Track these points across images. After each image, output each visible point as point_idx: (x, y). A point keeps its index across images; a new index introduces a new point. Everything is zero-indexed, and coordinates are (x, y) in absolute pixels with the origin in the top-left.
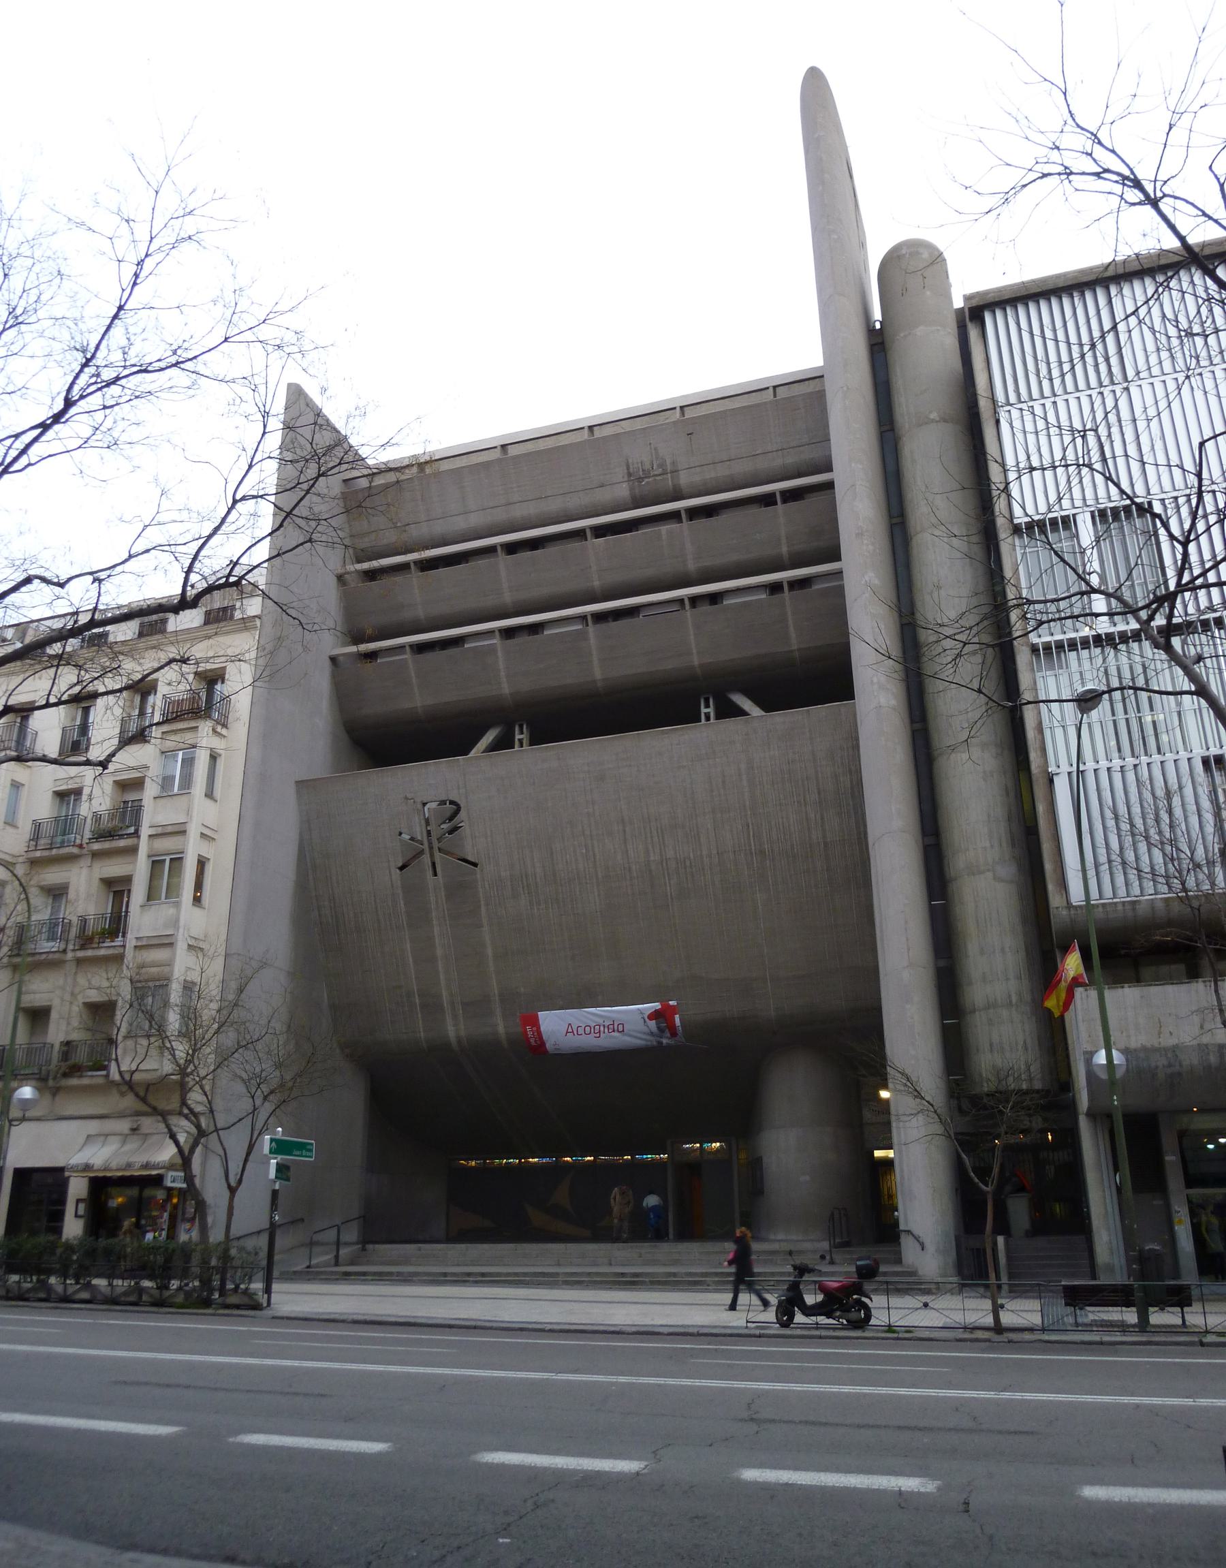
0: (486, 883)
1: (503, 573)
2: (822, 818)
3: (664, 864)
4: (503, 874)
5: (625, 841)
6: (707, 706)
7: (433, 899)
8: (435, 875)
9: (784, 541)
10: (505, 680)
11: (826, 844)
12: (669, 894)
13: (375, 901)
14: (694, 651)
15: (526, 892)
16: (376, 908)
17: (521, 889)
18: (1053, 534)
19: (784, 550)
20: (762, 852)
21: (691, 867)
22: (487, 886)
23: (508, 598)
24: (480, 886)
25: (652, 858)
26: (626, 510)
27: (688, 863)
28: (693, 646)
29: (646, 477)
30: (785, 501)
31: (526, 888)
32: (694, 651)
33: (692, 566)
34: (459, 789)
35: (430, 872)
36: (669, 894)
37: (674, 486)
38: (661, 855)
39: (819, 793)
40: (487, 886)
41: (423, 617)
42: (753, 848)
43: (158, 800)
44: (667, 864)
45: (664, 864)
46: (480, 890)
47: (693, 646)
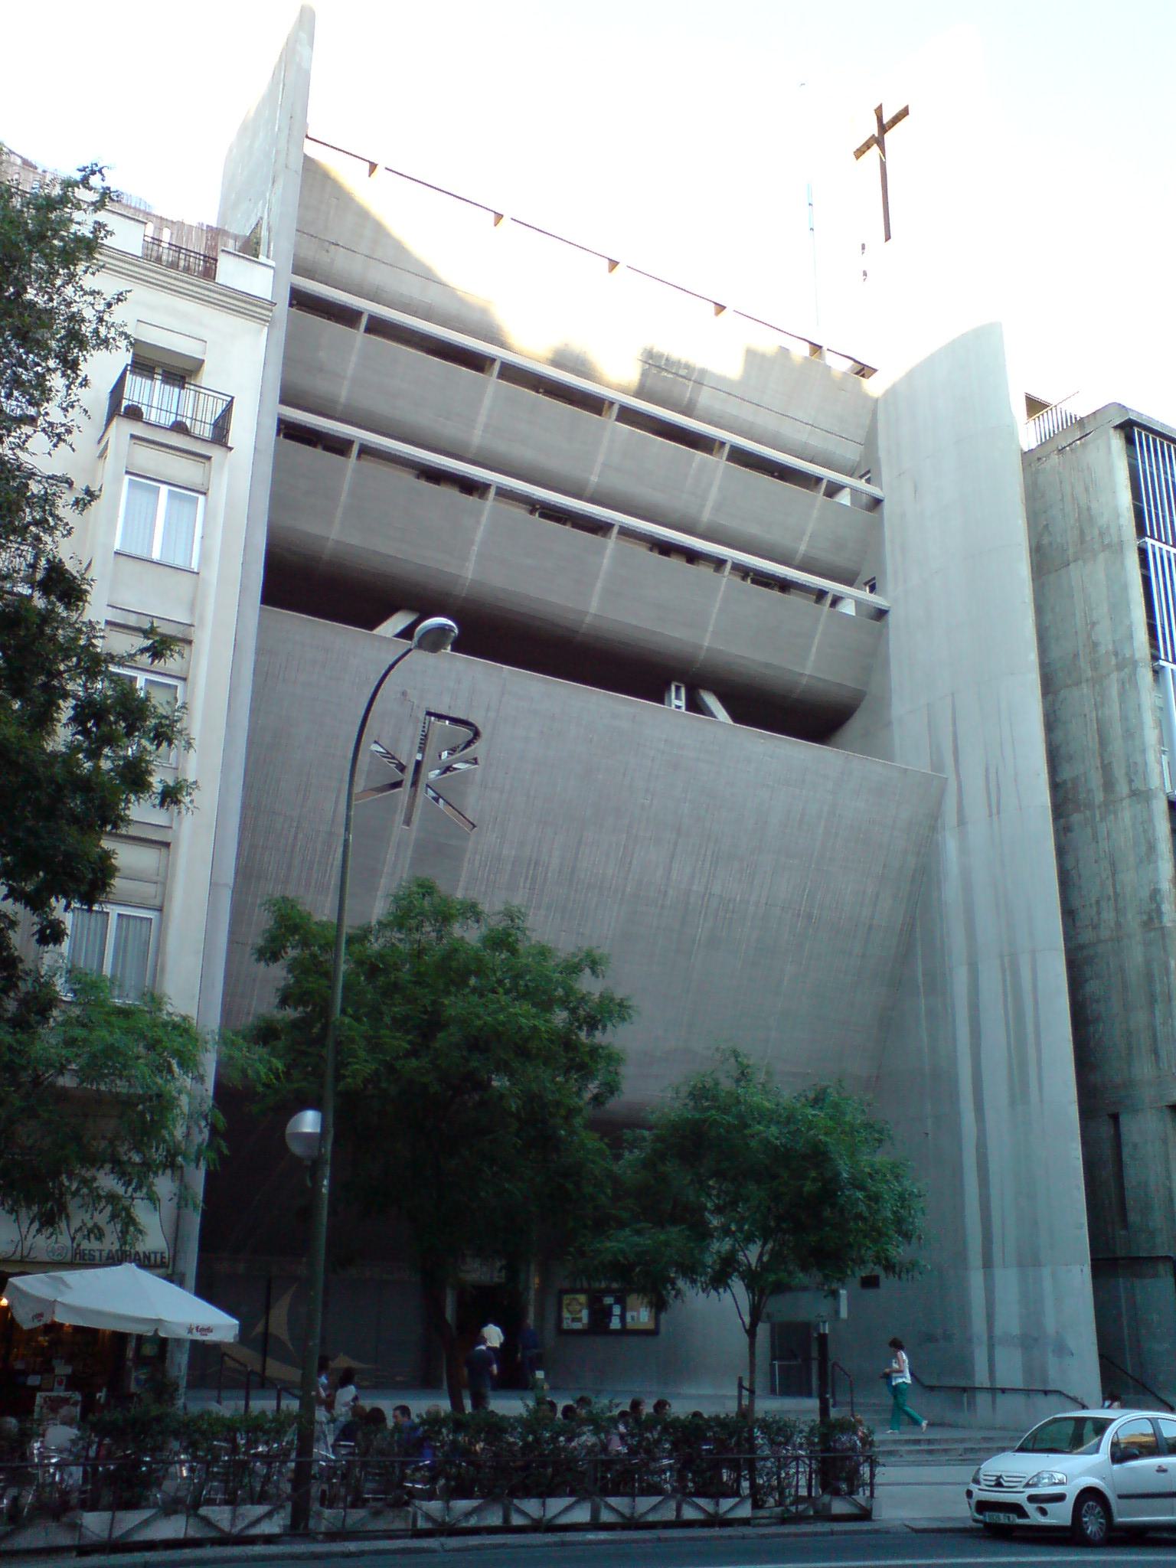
0: (478, 857)
1: (487, 402)
2: (877, 896)
3: (706, 898)
4: (505, 852)
5: (673, 857)
6: (678, 697)
7: (390, 856)
8: (408, 821)
9: (806, 538)
10: (474, 558)
11: (870, 927)
12: (698, 938)
13: (295, 837)
14: (711, 628)
15: (528, 885)
16: (294, 846)
17: (522, 880)
18: (731, 577)
19: (803, 548)
20: (809, 916)
21: (733, 912)
22: (477, 863)
23: (477, 438)
24: (466, 860)
25: (695, 888)
26: (802, 459)
27: (731, 906)
28: (712, 622)
29: (666, 370)
30: (502, 375)
31: (529, 881)
32: (711, 628)
33: (706, 516)
34: (488, 709)
35: (400, 817)
36: (698, 938)
37: (690, 399)
38: (706, 889)
39: (885, 866)
40: (477, 863)
41: (342, 400)
42: (802, 909)
43: (118, 556)
44: (708, 901)
45: (706, 898)
46: (466, 864)
47: (712, 622)
